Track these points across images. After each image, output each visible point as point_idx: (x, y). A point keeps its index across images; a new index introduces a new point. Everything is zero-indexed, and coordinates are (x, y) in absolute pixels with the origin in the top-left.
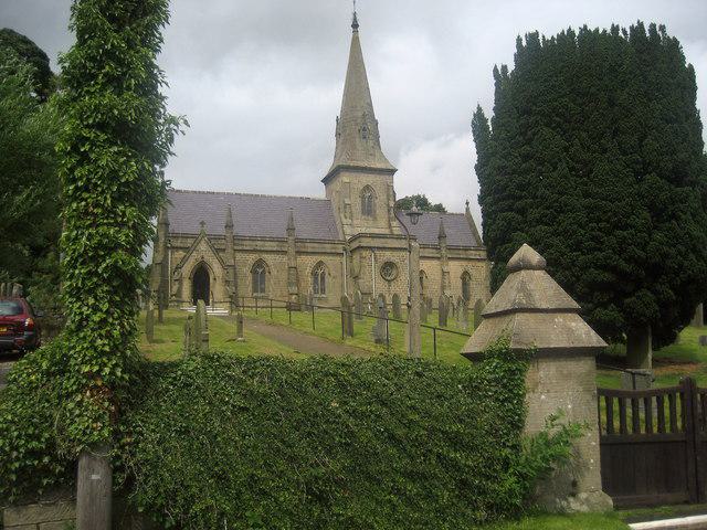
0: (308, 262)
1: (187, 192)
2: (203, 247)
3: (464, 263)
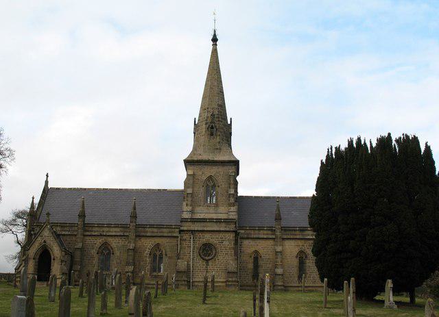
0: (148, 244)
1: (64, 189)
2: (46, 233)
3: (300, 243)
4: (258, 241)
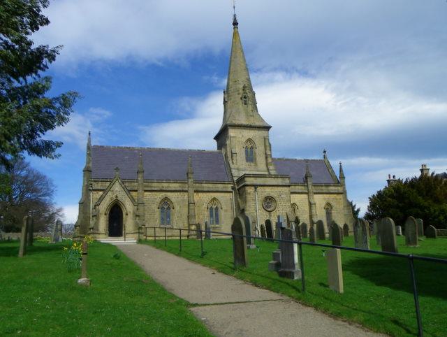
4: (265, 188)
